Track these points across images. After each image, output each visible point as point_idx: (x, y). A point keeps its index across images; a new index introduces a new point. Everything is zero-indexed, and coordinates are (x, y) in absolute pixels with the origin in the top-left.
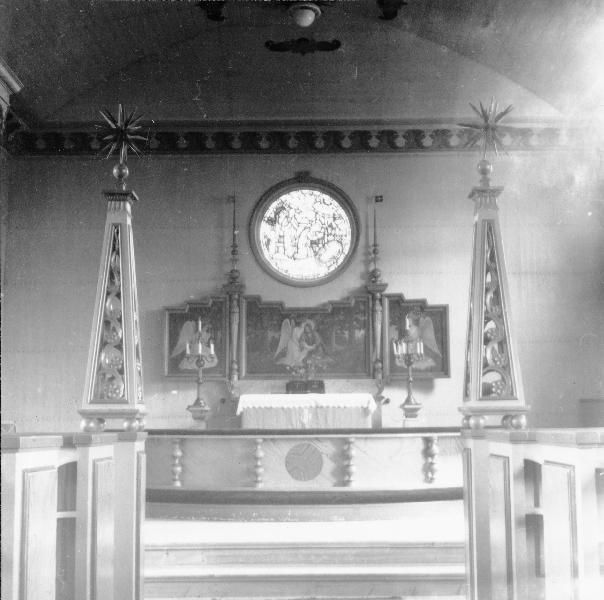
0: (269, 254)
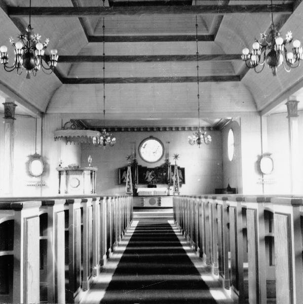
0: (143, 155)
